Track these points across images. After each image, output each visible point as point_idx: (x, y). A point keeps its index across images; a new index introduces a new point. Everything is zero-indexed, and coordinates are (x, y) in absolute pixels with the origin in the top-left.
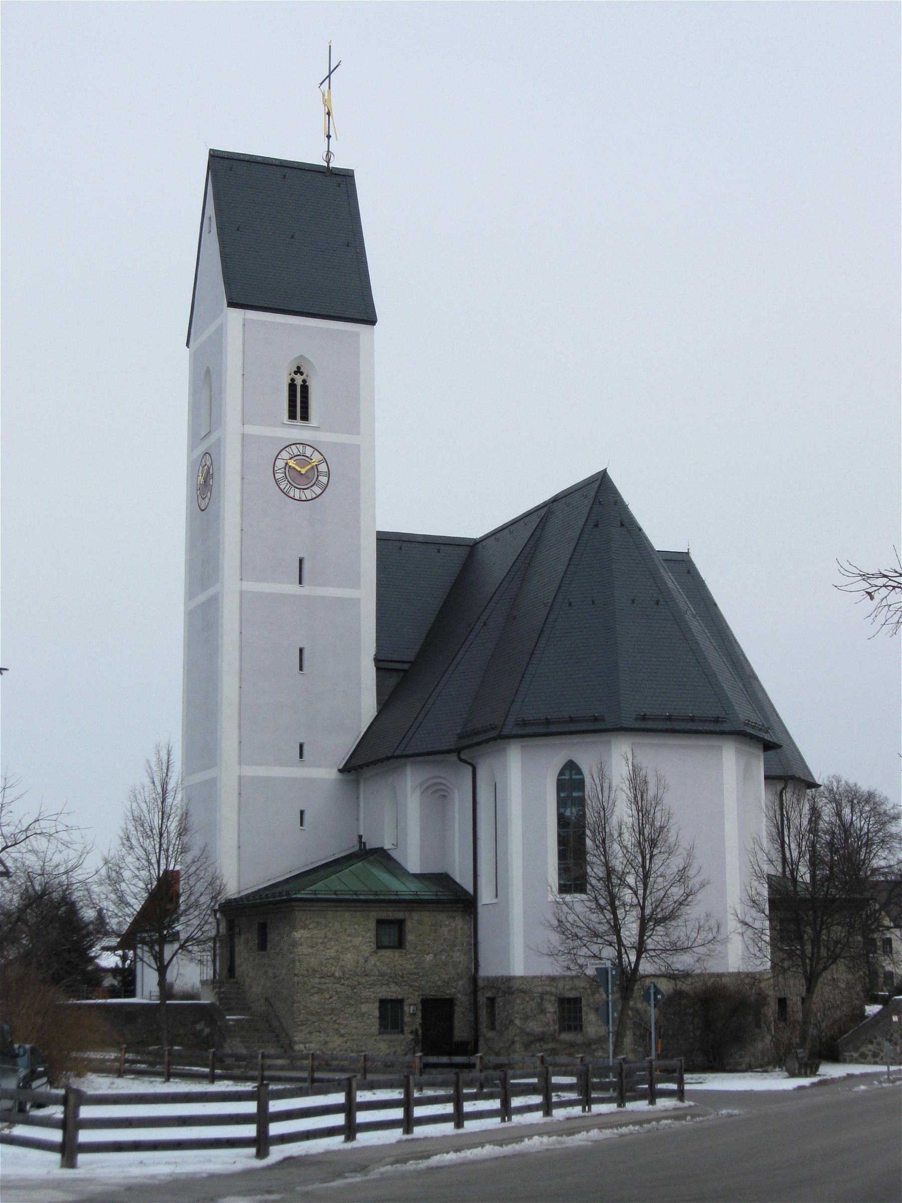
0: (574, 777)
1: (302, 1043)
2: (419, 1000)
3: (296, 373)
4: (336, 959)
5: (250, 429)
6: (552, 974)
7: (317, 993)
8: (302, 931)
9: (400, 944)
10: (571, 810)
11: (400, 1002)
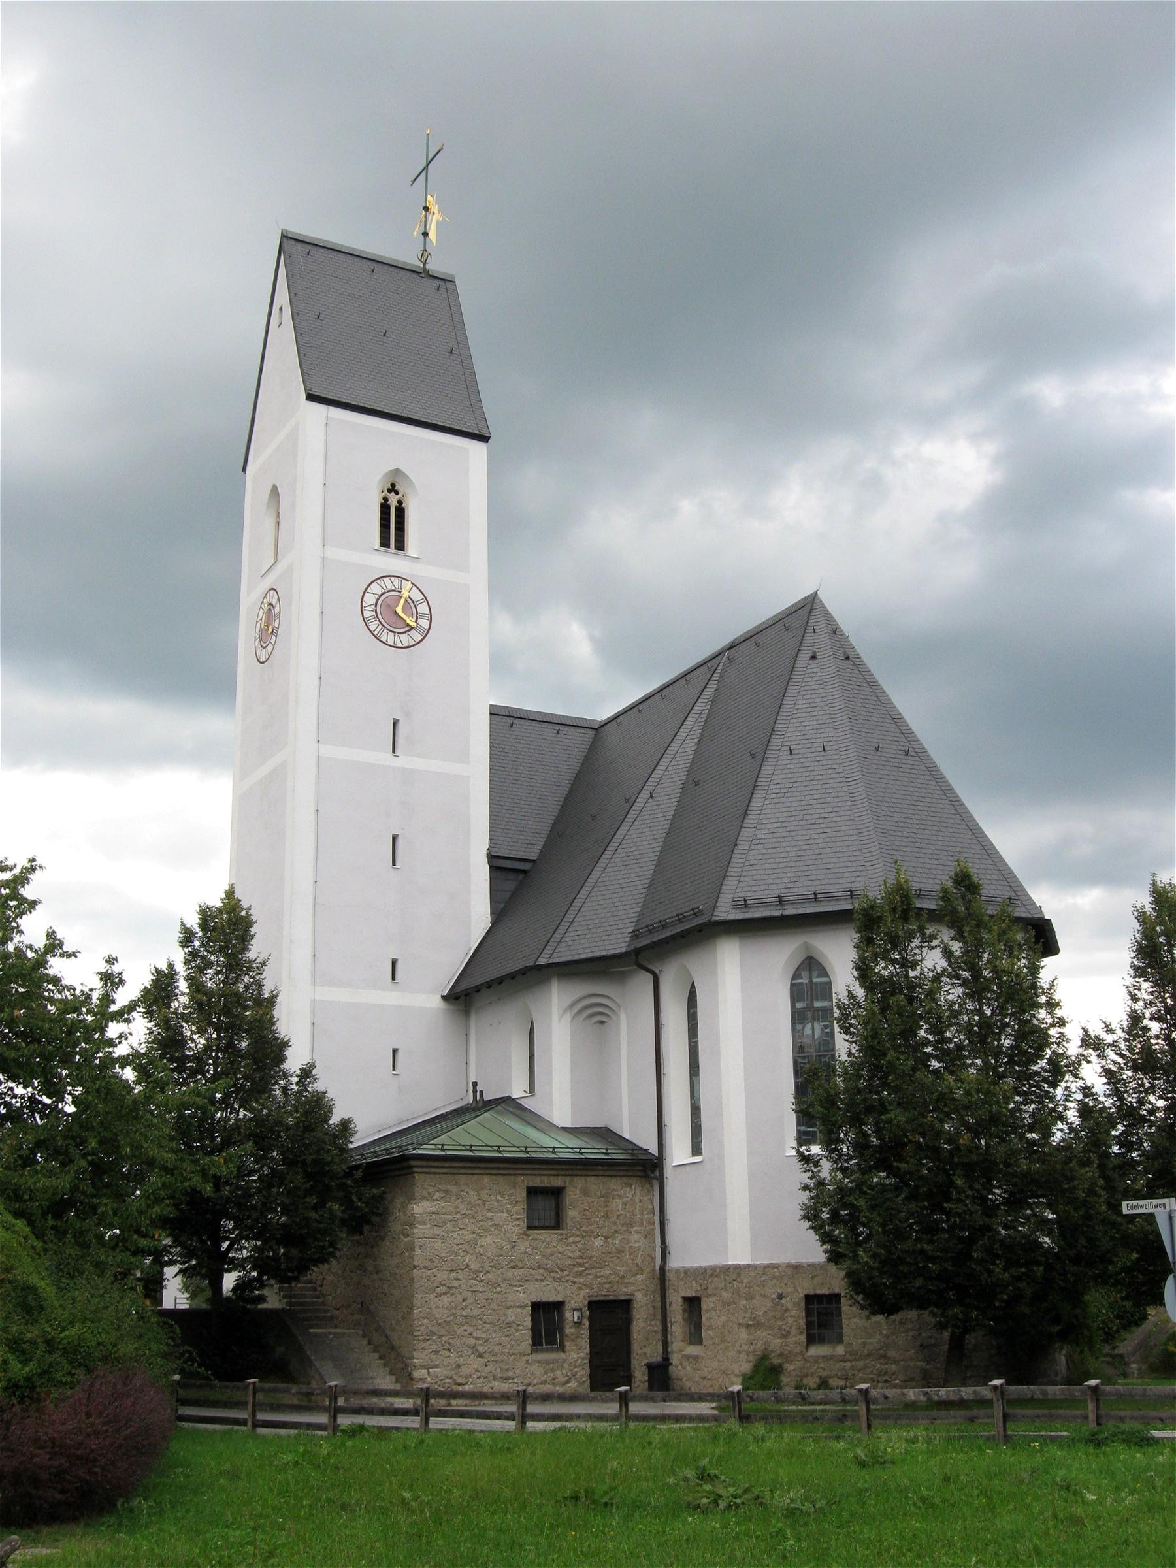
0: (815, 980)
1: (423, 1367)
2: (586, 1303)
3: (389, 491)
4: (473, 1243)
5: (332, 553)
6: (793, 1261)
7: (444, 1294)
8: (425, 1203)
9: (557, 1224)
10: (813, 1026)
11: (558, 1306)
